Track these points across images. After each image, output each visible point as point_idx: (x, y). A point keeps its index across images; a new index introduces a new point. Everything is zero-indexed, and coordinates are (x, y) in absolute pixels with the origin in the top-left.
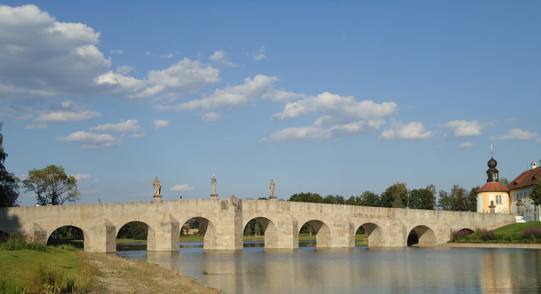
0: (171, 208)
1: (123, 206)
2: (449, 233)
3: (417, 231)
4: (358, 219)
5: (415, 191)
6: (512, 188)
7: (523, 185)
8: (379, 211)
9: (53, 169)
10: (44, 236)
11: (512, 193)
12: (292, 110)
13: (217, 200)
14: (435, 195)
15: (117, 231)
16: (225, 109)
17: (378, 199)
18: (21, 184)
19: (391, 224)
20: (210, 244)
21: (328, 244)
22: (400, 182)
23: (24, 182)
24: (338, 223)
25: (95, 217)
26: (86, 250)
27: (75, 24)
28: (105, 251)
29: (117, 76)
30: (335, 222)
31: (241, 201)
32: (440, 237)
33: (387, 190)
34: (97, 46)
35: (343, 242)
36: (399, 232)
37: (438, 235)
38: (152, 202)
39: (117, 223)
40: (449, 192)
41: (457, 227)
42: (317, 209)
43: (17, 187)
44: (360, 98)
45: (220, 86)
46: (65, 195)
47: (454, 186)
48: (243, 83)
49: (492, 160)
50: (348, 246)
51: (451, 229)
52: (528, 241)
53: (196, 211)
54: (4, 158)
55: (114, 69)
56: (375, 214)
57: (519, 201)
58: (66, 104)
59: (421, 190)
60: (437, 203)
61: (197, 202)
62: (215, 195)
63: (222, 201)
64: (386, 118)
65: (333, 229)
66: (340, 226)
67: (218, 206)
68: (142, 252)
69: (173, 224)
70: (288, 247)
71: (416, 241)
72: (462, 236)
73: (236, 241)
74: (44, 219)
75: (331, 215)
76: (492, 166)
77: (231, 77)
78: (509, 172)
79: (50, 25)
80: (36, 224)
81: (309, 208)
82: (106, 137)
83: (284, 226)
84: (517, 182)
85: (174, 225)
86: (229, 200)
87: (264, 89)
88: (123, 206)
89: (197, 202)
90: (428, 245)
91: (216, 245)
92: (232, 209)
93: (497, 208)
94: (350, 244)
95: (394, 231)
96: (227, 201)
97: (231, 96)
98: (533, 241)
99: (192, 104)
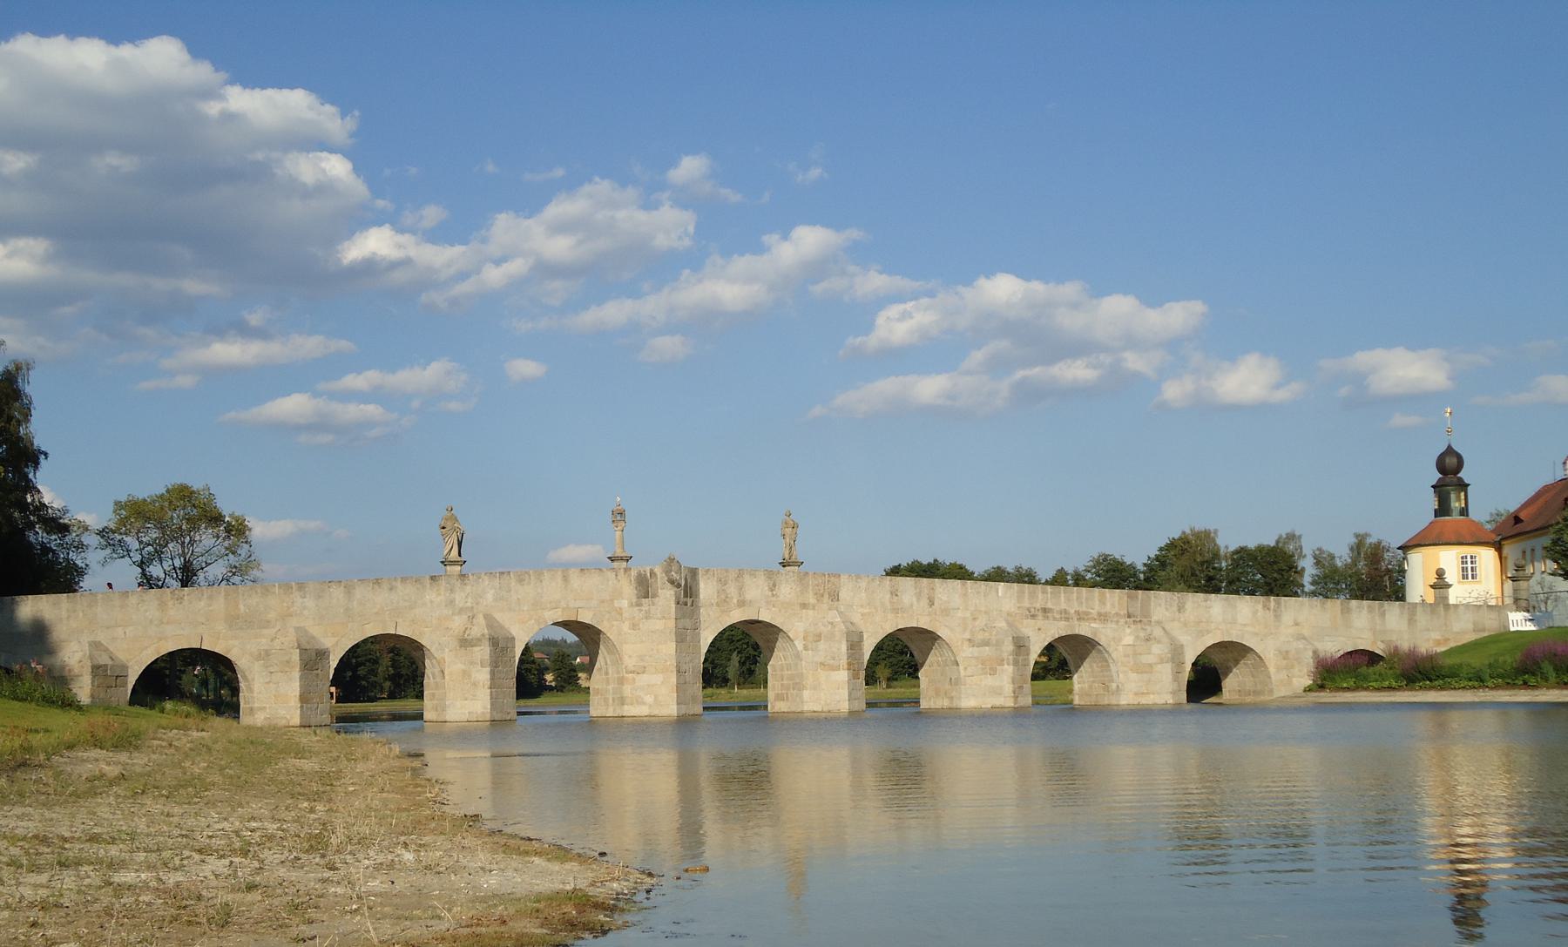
0: (490, 596)
1: (349, 590)
2: (1308, 663)
3: (1217, 659)
4: (1040, 622)
5: (1242, 551)
6: (1509, 533)
7: (1539, 524)
8: (1103, 602)
9: (183, 495)
10: (121, 677)
11: (1508, 549)
12: (898, 325)
13: (626, 570)
14: (1301, 564)
15: (334, 664)
16: (704, 324)
17: (1135, 575)
18: (91, 540)
19: (1137, 637)
20: (606, 700)
21: (951, 698)
22: (1200, 526)
23: (102, 533)
24: (980, 636)
25: (267, 624)
26: (245, 719)
27: (286, 92)
28: (296, 721)
29: (406, 239)
30: (972, 633)
31: (694, 572)
32: (1283, 675)
33: (1161, 549)
34: (347, 153)
35: (996, 691)
36: (1162, 661)
37: (1278, 669)
38: (433, 578)
39: (334, 640)
40: (1342, 554)
41: (1335, 646)
42: (919, 596)
43: (80, 547)
44: (1099, 290)
45: (690, 261)
46: (218, 570)
47: (1357, 536)
48: (760, 249)
49: (1450, 451)
50: (1010, 703)
51: (1315, 652)
52: (1532, 681)
53: (563, 604)
54: (36, 464)
55: (393, 220)
56: (1100, 614)
57: (1519, 568)
58: (255, 319)
59: (1260, 549)
60: (1308, 588)
61: (566, 579)
62: (622, 559)
63: (639, 574)
64: (1173, 345)
65: (965, 653)
66: (986, 643)
67: (629, 589)
68: (418, 723)
69: (494, 642)
70: (833, 707)
71: (1216, 688)
72: (1348, 670)
73: (681, 687)
74: (120, 631)
75: (960, 614)
76: (1450, 470)
77: (728, 230)
78: (1495, 491)
79: (209, 94)
80: (96, 645)
81: (894, 593)
82: (372, 410)
83: (822, 645)
84: (1522, 516)
85: (499, 645)
86: (658, 570)
87: (817, 269)
88: (349, 590)
89: (566, 579)
90: (1249, 699)
91: (622, 701)
92: (666, 596)
93: (1465, 589)
94: (1016, 698)
95: (1150, 659)
96: (652, 573)
97: (728, 287)
98: (1547, 680)
99: (614, 312)
